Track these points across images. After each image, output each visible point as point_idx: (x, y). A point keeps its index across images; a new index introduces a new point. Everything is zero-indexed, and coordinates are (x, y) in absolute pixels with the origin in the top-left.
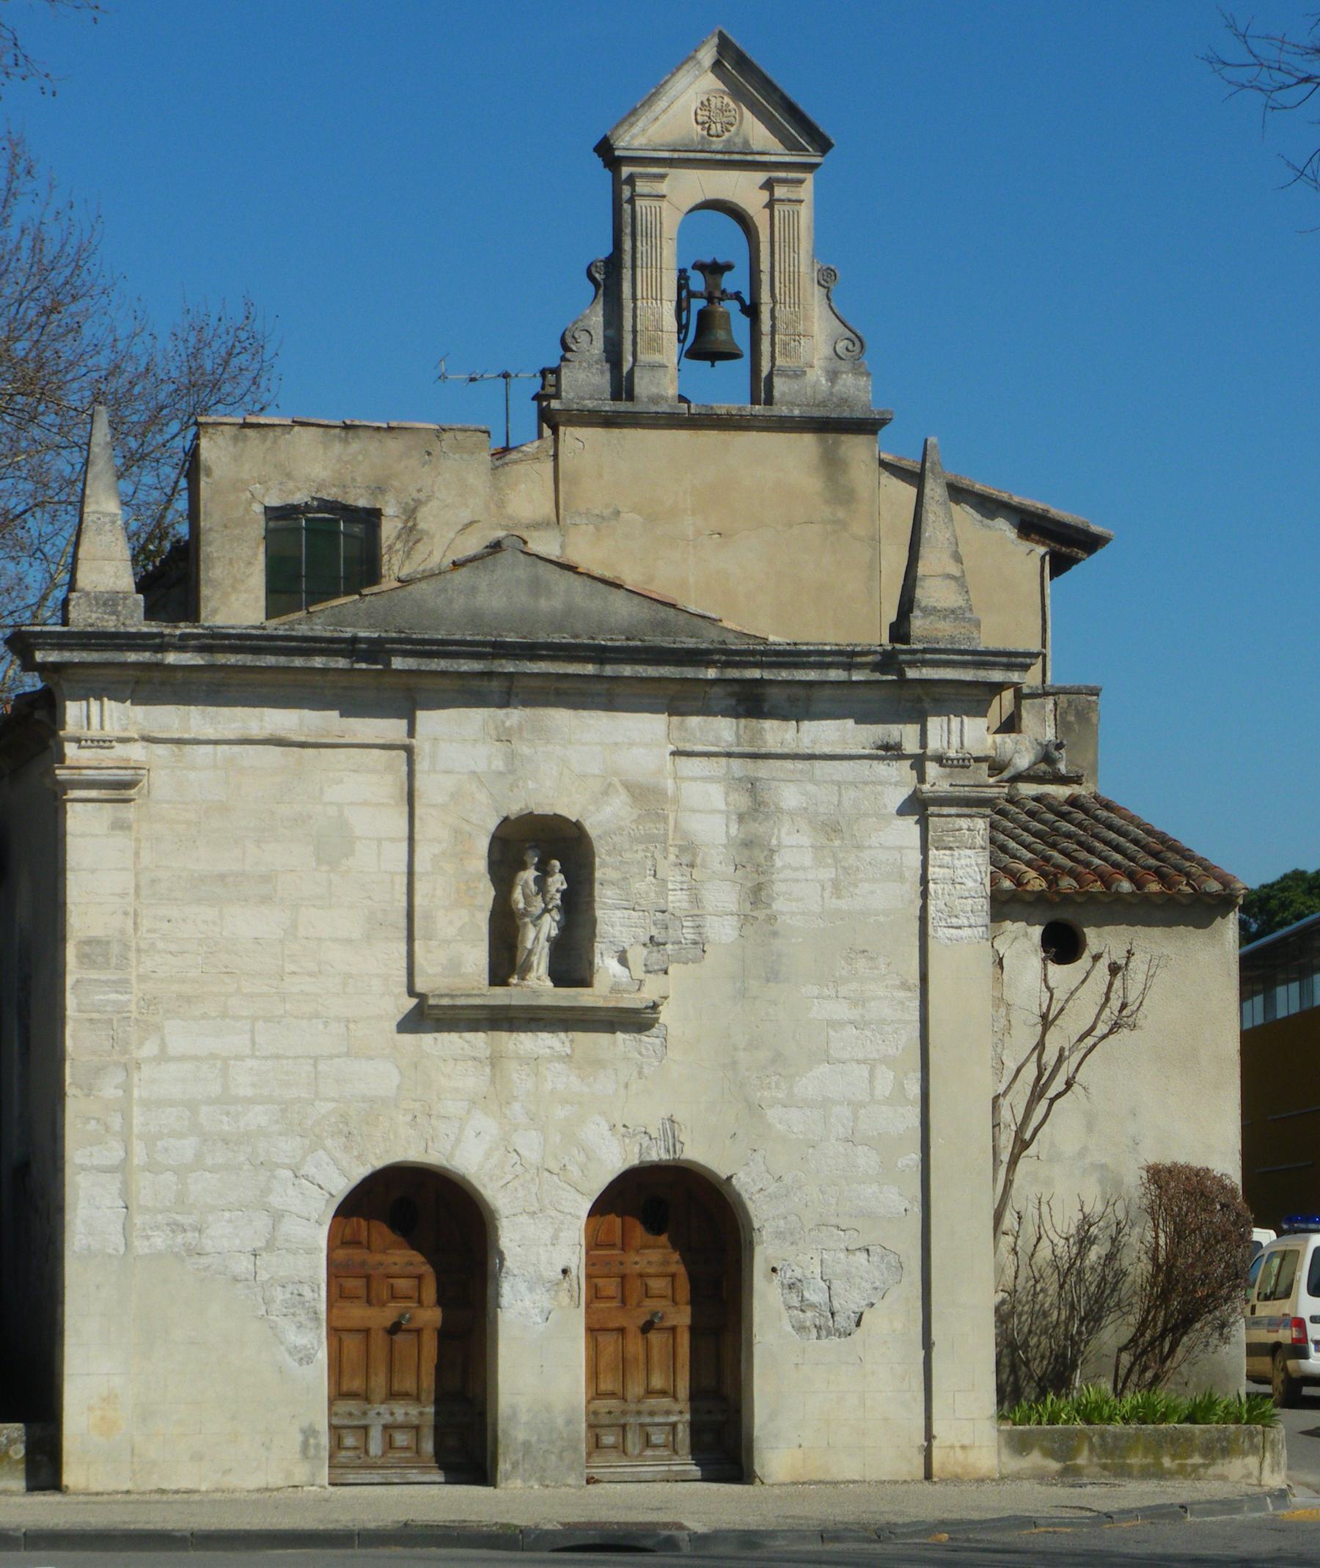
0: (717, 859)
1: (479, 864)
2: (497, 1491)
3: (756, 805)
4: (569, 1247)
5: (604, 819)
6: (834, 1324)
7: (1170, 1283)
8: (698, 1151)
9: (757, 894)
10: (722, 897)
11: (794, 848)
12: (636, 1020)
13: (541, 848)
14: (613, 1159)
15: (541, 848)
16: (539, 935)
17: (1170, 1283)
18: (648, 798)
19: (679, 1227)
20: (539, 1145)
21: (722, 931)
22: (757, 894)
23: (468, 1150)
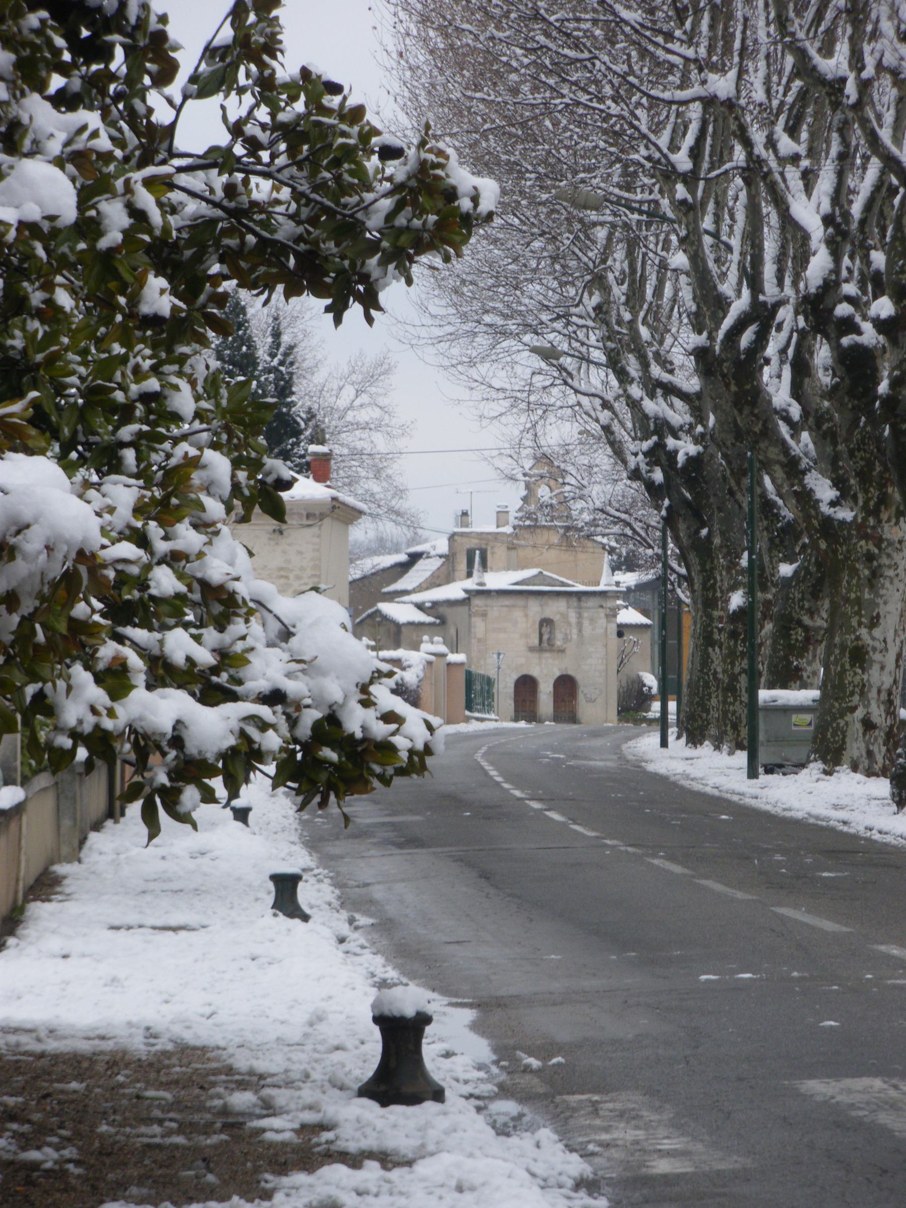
0: (574, 625)
1: (537, 626)
2: (83, 866)
3: (580, 616)
4: (511, 689)
5: (556, 618)
6: (591, 701)
7: (251, 1136)
8: (570, 673)
9: (580, 631)
10: (575, 631)
11: (586, 623)
12: (562, 651)
13: (546, 623)
14: (557, 674)
15: (546, 623)
16: (545, 637)
17: (251, 1136)
18: (565, 616)
19: (566, 686)
20: (545, 674)
21: (575, 637)
22: (580, 631)
23: (535, 672)
